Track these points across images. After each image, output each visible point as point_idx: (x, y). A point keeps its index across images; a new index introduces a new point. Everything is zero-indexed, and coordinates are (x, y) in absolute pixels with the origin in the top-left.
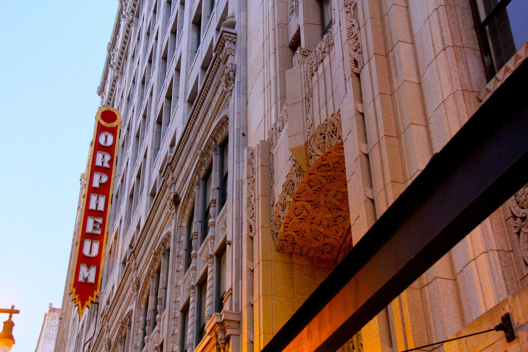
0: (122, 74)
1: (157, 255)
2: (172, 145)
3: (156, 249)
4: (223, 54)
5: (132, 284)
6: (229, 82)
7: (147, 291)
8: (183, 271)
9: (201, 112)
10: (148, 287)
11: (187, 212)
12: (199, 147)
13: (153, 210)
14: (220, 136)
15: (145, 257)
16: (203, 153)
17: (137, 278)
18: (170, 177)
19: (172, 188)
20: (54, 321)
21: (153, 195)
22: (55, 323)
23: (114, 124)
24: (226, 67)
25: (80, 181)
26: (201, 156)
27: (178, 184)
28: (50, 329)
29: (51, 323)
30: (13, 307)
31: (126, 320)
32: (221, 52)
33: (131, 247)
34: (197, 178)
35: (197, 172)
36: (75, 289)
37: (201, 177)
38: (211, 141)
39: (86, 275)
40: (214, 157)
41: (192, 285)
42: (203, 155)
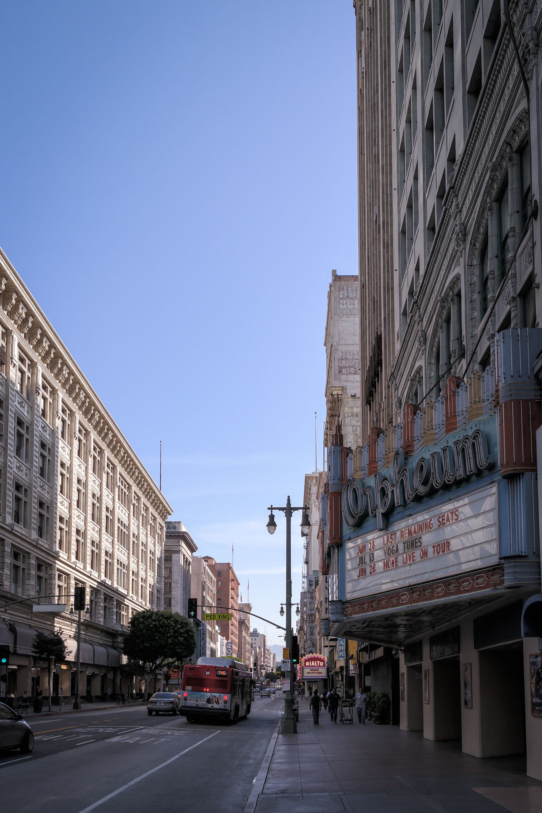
2: (452, 159)
3: (412, 375)
4: (518, 13)
5: (454, 236)
6: (528, 57)
7: (436, 344)
8: (478, 318)
9: (471, 163)
10: (437, 340)
11: (434, 350)
13: (433, 255)
14: (517, 138)
15: (431, 305)
17: (398, 398)
18: (454, 204)
19: (458, 217)
20: (341, 293)
21: (431, 228)
22: (344, 294)
24: (524, 35)
26: (492, 171)
27: (464, 213)
28: (339, 303)
29: (339, 295)
30: (272, 506)
31: (416, 377)
32: (451, 207)
33: (411, 293)
37: (493, 198)
38: (504, 147)
40: (509, 170)
41: (491, 334)
42: (494, 169)
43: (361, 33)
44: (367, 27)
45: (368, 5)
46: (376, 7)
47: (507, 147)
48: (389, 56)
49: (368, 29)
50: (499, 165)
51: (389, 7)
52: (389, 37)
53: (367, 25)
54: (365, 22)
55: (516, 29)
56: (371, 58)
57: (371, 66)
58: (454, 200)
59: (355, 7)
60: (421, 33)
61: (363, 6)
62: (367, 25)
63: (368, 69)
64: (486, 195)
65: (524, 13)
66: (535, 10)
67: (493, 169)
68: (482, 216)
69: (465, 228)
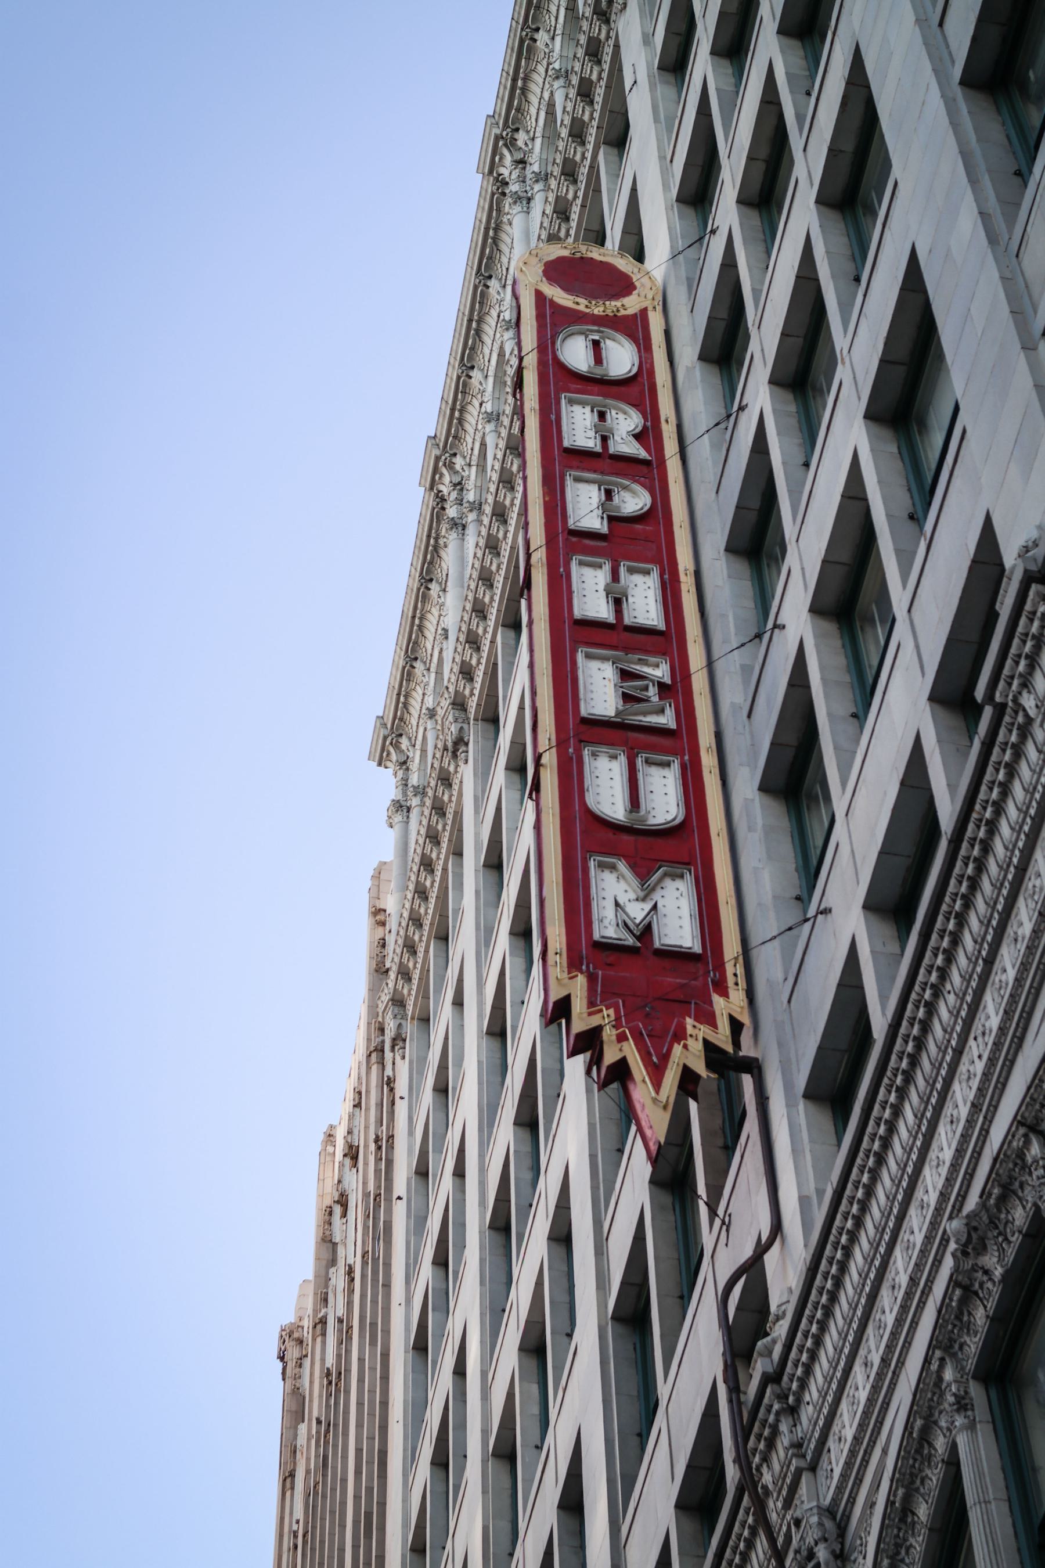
0: (446, 939)
1: (982, 1248)
12: (950, 1200)
16: (971, 1226)
18: (784, 1441)
23: (631, 304)
24: (798, 1523)
25: (280, 1365)
26: (963, 1252)
34: (948, 1375)
35: (944, 1343)
36: (581, 980)
37: (970, 1365)
39: (638, 912)
43: (296, 1428)
44: (315, 1414)
45: (323, 1360)
46: (348, 1371)
47: (1027, 1143)
48: (382, 1505)
49: (319, 1422)
50: (993, 1223)
51: (385, 1378)
52: (383, 1454)
53: (315, 1408)
54: (311, 1401)
55: (774, 1506)
56: (324, 1496)
57: (323, 1519)
58: (783, 1427)
59: (282, 1358)
60: (484, 1462)
61: (307, 1362)
62: (315, 1408)
63: (314, 1527)
64: (938, 1353)
65: (792, 1468)
66: (824, 1464)
67: (965, 1245)
68: (919, 1451)
69: (842, 1529)
